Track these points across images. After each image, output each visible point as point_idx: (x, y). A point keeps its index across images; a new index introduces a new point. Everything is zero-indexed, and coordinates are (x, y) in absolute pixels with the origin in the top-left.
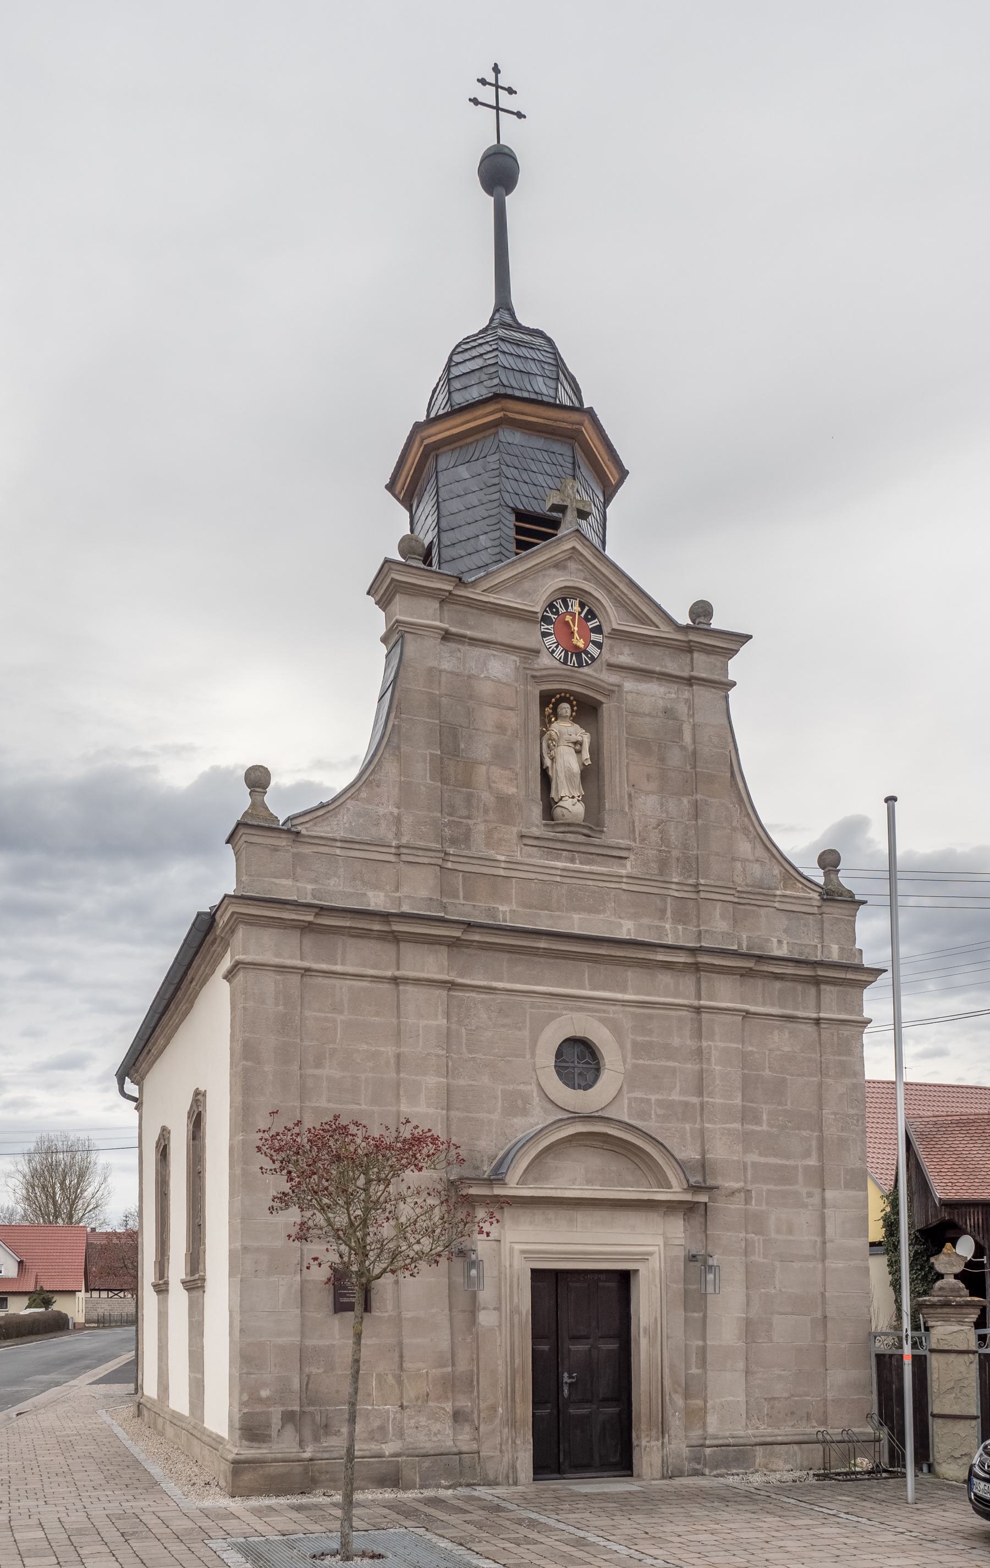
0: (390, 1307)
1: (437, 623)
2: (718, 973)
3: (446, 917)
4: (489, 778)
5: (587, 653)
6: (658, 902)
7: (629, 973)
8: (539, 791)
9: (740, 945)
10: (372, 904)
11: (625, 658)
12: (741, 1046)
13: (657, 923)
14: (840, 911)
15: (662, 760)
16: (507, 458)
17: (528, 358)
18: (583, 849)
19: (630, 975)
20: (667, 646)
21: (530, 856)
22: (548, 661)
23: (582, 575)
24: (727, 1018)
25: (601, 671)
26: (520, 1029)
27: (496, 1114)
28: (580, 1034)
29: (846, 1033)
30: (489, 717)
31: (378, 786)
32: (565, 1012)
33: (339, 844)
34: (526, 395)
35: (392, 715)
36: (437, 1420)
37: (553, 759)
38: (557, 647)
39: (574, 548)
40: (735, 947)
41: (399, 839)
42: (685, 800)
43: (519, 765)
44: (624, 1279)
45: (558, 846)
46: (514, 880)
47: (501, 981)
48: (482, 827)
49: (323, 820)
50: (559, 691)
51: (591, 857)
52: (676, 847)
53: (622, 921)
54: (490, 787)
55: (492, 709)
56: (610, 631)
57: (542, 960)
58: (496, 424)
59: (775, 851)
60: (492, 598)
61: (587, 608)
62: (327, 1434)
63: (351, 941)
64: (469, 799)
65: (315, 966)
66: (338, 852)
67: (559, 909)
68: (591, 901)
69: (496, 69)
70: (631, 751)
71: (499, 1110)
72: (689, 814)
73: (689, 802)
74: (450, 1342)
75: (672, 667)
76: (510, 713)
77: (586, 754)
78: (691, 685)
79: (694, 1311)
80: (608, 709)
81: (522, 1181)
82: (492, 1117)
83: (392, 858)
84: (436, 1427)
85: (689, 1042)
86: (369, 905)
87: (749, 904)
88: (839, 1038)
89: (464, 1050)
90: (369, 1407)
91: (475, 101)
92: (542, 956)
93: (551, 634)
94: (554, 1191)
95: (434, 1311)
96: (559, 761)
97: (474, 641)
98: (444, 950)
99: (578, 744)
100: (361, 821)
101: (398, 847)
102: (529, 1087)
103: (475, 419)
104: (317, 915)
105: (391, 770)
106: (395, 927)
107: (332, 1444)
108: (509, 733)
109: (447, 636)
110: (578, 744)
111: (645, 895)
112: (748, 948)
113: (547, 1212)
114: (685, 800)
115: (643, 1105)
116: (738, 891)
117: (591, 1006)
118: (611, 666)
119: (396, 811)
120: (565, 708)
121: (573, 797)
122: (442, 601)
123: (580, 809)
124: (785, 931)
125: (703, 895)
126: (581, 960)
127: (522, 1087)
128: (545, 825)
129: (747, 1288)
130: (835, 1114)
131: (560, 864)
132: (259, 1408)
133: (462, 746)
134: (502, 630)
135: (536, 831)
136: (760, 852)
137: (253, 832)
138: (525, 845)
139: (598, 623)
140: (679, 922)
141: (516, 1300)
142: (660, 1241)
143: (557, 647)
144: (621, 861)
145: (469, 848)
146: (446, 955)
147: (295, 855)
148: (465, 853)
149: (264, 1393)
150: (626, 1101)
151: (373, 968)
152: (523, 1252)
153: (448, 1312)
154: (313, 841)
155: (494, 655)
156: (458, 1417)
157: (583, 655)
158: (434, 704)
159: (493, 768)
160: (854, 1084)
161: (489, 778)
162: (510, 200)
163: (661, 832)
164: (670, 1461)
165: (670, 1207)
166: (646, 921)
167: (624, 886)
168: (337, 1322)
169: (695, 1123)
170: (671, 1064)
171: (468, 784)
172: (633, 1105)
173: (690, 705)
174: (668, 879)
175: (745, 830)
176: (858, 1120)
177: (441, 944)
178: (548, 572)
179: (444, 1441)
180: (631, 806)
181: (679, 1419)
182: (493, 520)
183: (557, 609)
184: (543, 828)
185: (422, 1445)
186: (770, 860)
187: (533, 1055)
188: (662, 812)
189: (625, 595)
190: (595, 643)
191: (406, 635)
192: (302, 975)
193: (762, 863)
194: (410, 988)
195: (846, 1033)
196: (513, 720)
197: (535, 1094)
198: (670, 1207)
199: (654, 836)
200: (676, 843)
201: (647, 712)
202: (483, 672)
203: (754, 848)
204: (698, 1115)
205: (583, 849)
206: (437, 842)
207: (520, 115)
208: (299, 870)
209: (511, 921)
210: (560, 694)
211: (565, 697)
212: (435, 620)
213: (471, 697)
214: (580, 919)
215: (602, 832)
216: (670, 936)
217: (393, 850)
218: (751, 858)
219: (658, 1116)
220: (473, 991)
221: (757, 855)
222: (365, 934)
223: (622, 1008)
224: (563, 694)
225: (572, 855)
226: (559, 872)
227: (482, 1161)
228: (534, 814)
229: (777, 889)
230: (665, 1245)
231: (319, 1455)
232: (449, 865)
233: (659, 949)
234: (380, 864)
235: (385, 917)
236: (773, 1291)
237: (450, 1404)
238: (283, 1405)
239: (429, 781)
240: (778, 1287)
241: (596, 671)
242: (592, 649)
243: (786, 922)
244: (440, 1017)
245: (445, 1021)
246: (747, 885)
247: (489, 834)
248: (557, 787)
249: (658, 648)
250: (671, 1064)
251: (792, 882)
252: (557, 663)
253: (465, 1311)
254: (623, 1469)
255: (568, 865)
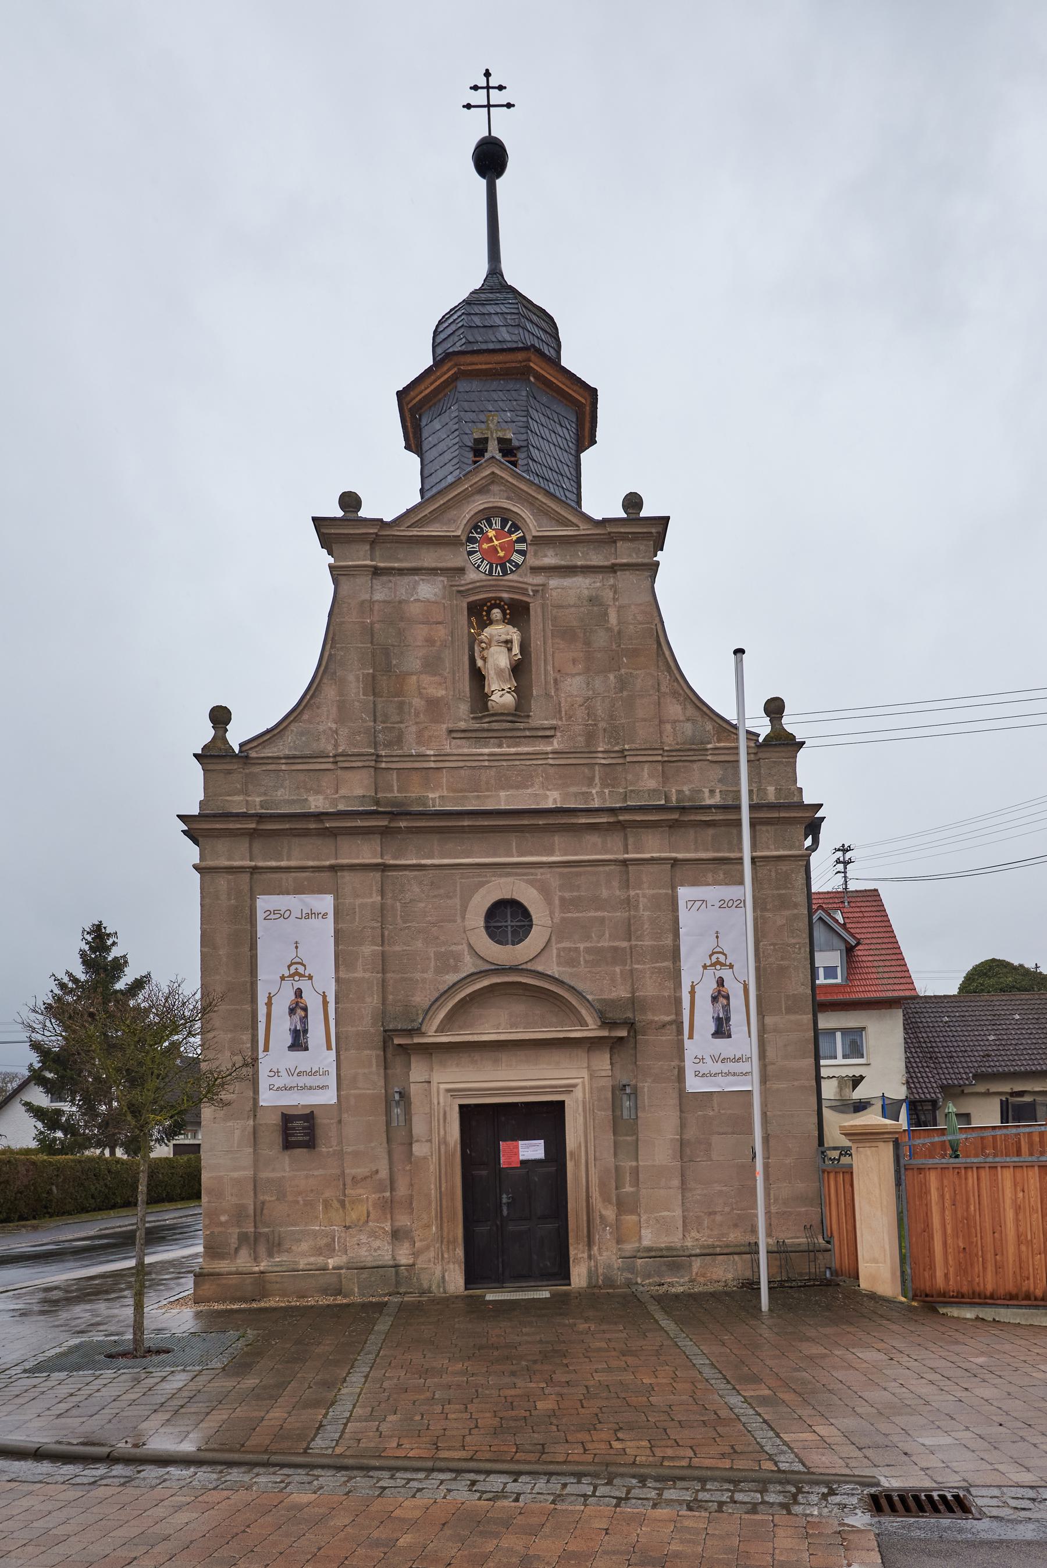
0: (334, 1142)
1: (368, 562)
2: (644, 827)
3: (380, 809)
4: (419, 686)
5: (510, 561)
6: (586, 771)
7: (556, 838)
8: (467, 689)
9: (667, 798)
10: (313, 807)
11: (550, 558)
12: (670, 892)
13: (585, 789)
14: (777, 754)
15: (588, 643)
16: (466, 405)
17: (491, 314)
18: (509, 734)
19: (557, 839)
20: (589, 542)
21: (459, 747)
22: (475, 575)
23: (505, 495)
24: (654, 868)
25: (526, 575)
26: (451, 898)
27: (429, 973)
28: (508, 896)
29: (784, 868)
30: (419, 633)
31: (318, 708)
32: (493, 879)
33: (283, 761)
34: (491, 346)
35: (328, 647)
36: (376, 1237)
37: (484, 659)
38: (482, 562)
39: (493, 473)
40: (663, 802)
41: (337, 749)
42: (611, 677)
43: (447, 670)
44: (461, 1106)
45: (485, 735)
46: (444, 770)
47: (433, 858)
48: (414, 729)
49: (271, 743)
50: (489, 599)
51: (518, 740)
52: (603, 719)
53: (548, 793)
54: (420, 693)
55: (421, 626)
56: (531, 538)
57: (470, 835)
58: (454, 378)
59: (705, 709)
60: (415, 532)
61: (510, 523)
62: (279, 1252)
63: (296, 840)
64: (401, 706)
65: (261, 864)
66: (283, 767)
67: (488, 790)
68: (519, 779)
69: (487, 74)
70: (557, 640)
71: (432, 970)
72: (615, 688)
73: (615, 677)
74: (388, 1171)
75: (596, 559)
76: (440, 627)
77: (516, 650)
78: (615, 572)
79: (627, 1135)
80: (535, 609)
81: (441, 1029)
82: (425, 975)
83: (330, 766)
84: (377, 1243)
85: (618, 893)
86: (310, 808)
87: (680, 761)
88: (777, 873)
89: (399, 921)
90: (317, 1228)
91: (468, 106)
92: (469, 833)
93: (477, 551)
94: (470, 1036)
95: (373, 1145)
96: (490, 661)
97: (401, 572)
98: (377, 839)
99: (508, 643)
100: (304, 738)
101: (335, 756)
102: (460, 947)
103: (439, 378)
104: (258, 823)
105: (330, 692)
106: (621, 818)
107: (285, 1259)
108: (438, 644)
109: (377, 572)
110: (508, 643)
111: (572, 767)
112: (678, 801)
113: (472, 1055)
114: (611, 677)
115: (572, 953)
116: (667, 751)
117: (518, 871)
118: (535, 570)
119: (334, 726)
120: (496, 613)
121: (503, 690)
122: (373, 543)
123: (509, 699)
124: (720, 781)
125: (628, 759)
126: (509, 832)
127: (454, 948)
128: (473, 718)
129: (681, 1111)
130: (774, 944)
131: (486, 751)
132: (217, 1230)
133: (394, 662)
134: (429, 558)
135: (462, 725)
136: (691, 711)
137: (214, 761)
138: (454, 738)
139: (522, 534)
140: (607, 786)
141: (442, 1132)
142: (585, 1074)
143: (482, 562)
144: (547, 740)
145: (402, 749)
146: (379, 842)
147: (246, 774)
148: (400, 752)
149: (223, 1218)
150: (555, 951)
151: (314, 859)
152: (448, 1091)
153: (386, 1146)
154: (315, 760)
155: (423, 580)
156: (396, 1235)
157: (508, 564)
158: (369, 632)
159: (423, 677)
160: (795, 915)
161: (419, 686)
162: (500, 183)
163: (587, 708)
164: (600, 1271)
165: (591, 1044)
166: (573, 789)
167: (551, 762)
168: (287, 1158)
169: (626, 965)
170: (599, 914)
171: (399, 693)
172: (562, 954)
173: (614, 588)
174: (593, 749)
175: (675, 694)
176: (800, 948)
177: (374, 834)
178: (473, 498)
179: (383, 1256)
180: (557, 690)
181: (611, 1233)
182: (455, 461)
183: (482, 529)
184: (471, 721)
185: (363, 1259)
186: (702, 717)
187: (463, 918)
188: (588, 690)
189: (545, 504)
190: (518, 552)
191: (340, 577)
192: (252, 873)
193: (695, 722)
194: (346, 874)
195: (784, 868)
196: (441, 633)
197: (466, 953)
198: (591, 1044)
199: (580, 713)
200: (603, 716)
201: (572, 603)
202: (412, 595)
203: (685, 709)
204: (629, 957)
205: (509, 734)
206: (370, 747)
207: (509, 106)
208: (250, 787)
209: (505, 805)
210: (490, 601)
211: (497, 603)
212: (366, 560)
213: (402, 619)
214: (506, 795)
215: (528, 716)
216: (596, 800)
217: (331, 760)
218: (682, 718)
219: (586, 961)
220: (405, 870)
221: (688, 715)
222: (306, 833)
223: (549, 870)
224: (493, 602)
225: (500, 740)
226: (486, 758)
227: (418, 1014)
228: (461, 711)
229: (709, 743)
230: (592, 1077)
231: (270, 1269)
232: (383, 765)
233: (579, 814)
234: (322, 772)
235: (319, 816)
236: (711, 1113)
237: (389, 1224)
238: (239, 1227)
239: (362, 697)
240: (716, 1110)
241: (521, 576)
242: (518, 558)
243: (721, 772)
244: (374, 895)
245: (379, 898)
246: (677, 744)
247: (420, 734)
248: (489, 684)
249: (582, 545)
250: (599, 914)
251: (726, 734)
252: (483, 576)
253: (404, 1144)
254: (563, 1279)
255: (496, 750)
